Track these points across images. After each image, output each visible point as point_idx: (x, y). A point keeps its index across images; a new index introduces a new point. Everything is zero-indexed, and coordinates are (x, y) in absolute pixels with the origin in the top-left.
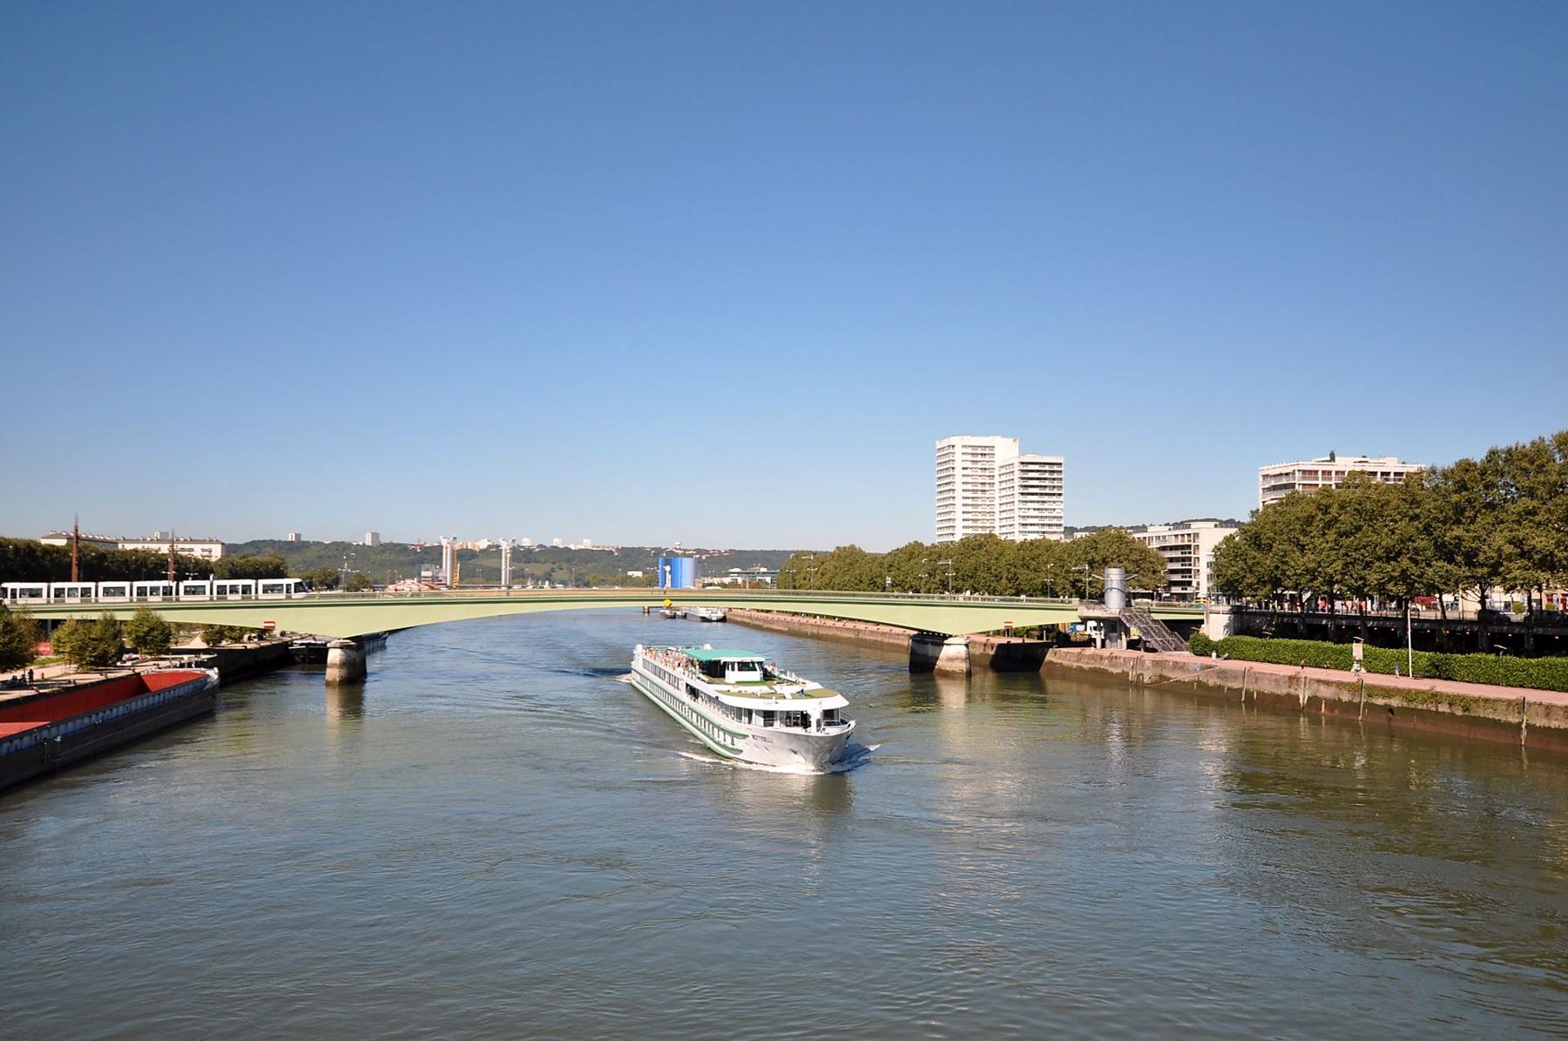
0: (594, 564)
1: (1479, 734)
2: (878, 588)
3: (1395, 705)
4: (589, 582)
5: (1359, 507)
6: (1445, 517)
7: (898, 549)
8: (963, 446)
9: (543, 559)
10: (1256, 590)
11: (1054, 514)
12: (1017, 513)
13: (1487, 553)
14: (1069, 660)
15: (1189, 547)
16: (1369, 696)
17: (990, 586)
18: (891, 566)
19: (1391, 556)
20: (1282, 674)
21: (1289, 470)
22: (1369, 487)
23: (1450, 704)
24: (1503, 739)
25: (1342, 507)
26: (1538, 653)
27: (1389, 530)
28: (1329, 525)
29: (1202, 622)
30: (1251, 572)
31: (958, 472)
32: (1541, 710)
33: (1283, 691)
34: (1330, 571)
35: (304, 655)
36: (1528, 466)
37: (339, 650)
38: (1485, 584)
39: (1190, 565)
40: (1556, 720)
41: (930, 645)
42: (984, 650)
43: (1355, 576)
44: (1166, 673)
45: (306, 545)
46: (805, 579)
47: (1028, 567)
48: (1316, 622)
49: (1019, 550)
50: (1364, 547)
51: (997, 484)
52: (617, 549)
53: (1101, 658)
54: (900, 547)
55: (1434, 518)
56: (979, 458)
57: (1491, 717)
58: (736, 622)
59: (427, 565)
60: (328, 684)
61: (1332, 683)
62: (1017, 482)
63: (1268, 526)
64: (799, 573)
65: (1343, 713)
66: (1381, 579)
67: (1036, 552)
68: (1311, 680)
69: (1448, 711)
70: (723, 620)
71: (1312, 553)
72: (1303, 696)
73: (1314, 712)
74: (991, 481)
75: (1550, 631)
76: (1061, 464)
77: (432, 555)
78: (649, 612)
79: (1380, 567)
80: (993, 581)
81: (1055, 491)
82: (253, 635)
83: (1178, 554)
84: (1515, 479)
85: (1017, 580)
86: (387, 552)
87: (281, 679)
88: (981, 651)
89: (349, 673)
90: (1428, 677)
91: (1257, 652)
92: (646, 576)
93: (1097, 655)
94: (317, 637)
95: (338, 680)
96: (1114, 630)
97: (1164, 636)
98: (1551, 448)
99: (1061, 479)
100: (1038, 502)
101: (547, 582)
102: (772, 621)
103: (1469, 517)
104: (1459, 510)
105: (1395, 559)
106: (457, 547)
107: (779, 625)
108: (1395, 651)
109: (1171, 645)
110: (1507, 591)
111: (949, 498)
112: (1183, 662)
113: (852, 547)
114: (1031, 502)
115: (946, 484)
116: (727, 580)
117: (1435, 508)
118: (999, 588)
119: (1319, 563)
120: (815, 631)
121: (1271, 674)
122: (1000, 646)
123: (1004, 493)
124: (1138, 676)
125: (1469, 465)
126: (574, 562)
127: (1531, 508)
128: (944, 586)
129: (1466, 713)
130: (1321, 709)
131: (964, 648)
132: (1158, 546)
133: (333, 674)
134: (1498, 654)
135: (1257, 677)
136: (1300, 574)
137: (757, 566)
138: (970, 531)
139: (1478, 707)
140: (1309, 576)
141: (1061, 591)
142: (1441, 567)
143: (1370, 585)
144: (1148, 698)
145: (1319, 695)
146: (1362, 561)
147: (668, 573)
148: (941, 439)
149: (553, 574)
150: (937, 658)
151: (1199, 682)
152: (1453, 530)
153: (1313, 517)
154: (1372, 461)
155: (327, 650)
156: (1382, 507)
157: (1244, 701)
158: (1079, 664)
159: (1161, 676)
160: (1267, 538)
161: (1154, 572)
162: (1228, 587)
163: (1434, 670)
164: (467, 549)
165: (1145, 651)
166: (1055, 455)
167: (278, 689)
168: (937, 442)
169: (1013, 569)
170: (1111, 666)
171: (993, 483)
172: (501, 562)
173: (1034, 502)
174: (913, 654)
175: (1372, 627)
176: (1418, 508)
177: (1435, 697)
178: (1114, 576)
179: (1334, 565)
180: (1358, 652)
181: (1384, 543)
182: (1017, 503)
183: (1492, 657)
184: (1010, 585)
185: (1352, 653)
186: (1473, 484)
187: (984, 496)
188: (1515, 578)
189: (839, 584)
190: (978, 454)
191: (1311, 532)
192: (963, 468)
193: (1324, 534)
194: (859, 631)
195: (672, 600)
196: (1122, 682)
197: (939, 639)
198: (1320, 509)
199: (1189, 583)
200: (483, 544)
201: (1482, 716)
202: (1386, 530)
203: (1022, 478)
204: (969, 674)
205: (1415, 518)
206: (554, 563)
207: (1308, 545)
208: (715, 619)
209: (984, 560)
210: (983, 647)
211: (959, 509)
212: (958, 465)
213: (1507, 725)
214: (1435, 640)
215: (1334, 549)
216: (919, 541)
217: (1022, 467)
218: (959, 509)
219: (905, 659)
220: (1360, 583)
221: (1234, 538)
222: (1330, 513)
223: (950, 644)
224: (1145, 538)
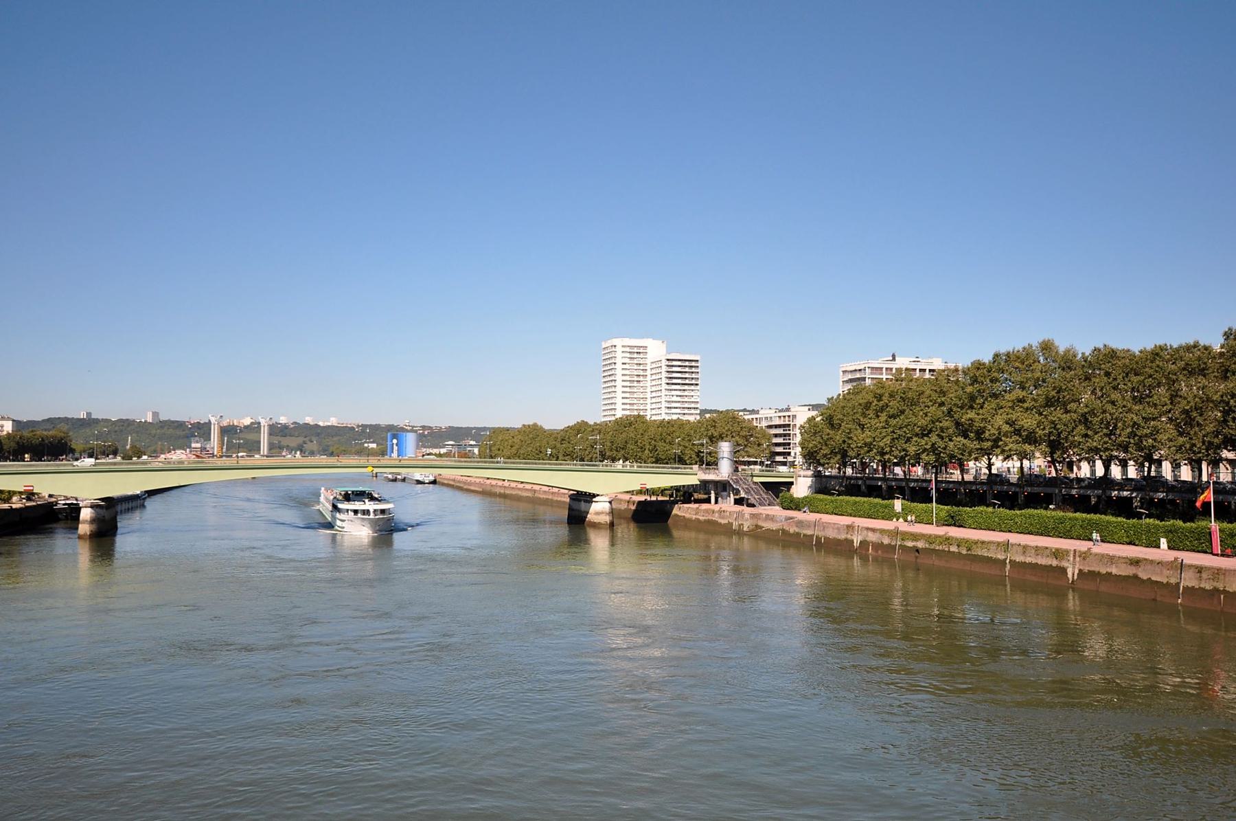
0: (339, 438)
1: (977, 568)
2: (553, 457)
3: (921, 547)
4: (333, 452)
5: (904, 396)
6: (962, 404)
7: (568, 427)
8: (623, 346)
9: (296, 434)
10: (829, 459)
11: (692, 400)
12: (663, 399)
13: (991, 431)
14: (690, 514)
15: (789, 425)
16: (902, 540)
17: (636, 455)
18: (563, 440)
19: (926, 433)
20: (842, 523)
21: (862, 367)
22: (911, 380)
23: (958, 546)
24: (995, 571)
25: (891, 396)
26: (869, 496)
27: (924, 413)
28: (882, 410)
29: (792, 483)
30: (826, 445)
31: (619, 366)
32: (1020, 549)
33: (843, 536)
34: (882, 444)
35: (66, 513)
36: (1020, 366)
37: (90, 509)
38: (988, 453)
39: (790, 439)
40: (1030, 556)
41: (582, 502)
42: (628, 505)
43: (899, 448)
44: (761, 523)
45: (97, 421)
46: (499, 450)
47: (665, 442)
48: (873, 483)
49: (658, 427)
50: (906, 426)
51: (649, 376)
52: (358, 426)
53: (713, 512)
54: (571, 425)
55: (955, 404)
56: (635, 356)
57: (986, 555)
58: (443, 484)
59: (197, 439)
60: (80, 537)
61: (877, 530)
62: (664, 375)
63: (838, 410)
64: (495, 445)
65: (883, 553)
66: (917, 451)
67: (671, 429)
68: (862, 528)
69: (957, 551)
70: (434, 482)
71: (870, 431)
72: (856, 540)
73: (864, 552)
74: (645, 374)
75: (1036, 490)
76: (697, 361)
77: (202, 430)
78: (376, 476)
79: (917, 442)
80: (639, 452)
81: (693, 382)
82: (23, 497)
83: (780, 431)
84: (1011, 375)
85: (656, 451)
86: (166, 428)
87: (50, 532)
88: (626, 507)
89: (98, 528)
90: (947, 525)
91: (827, 507)
92: (380, 447)
93: (710, 509)
94: (79, 499)
95: (88, 534)
96: (725, 490)
97: (761, 495)
98: (1036, 352)
99: (698, 373)
100: (680, 390)
101: (298, 453)
102: (470, 484)
103: (979, 404)
104: (972, 398)
105: (927, 435)
106: (225, 423)
107: (475, 487)
108: (924, 505)
109: (766, 501)
110: (1005, 459)
111: (611, 386)
112: (774, 514)
113: (535, 425)
114: (675, 390)
115: (610, 375)
116: (443, 451)
117: (955, 397)
118: (643, 457)
119: (874, 438)
120: (502, 491)
121: (834, 524)
122: (640, 503)
123: (654, 383)
124: (740, 525)
125: (980, 364)
126: (323, 436)
127: (1021, 397)
128: (603, 457)
129: (969, 552)
130: (869, 550)
131: (608, 504)
132: (766, 425)
133: (84, 528)
134: (994, 508)
135: (825, 526)
136: (861, 447)
137: (468, 439)
138: (628, 413)
139: (977, 547)
140: (866, 448)
141: (688, 459)
142: (959, 442)
143: (909, 455)
144: (747, 543)
145: (868, 539)
146: (905, 437)
147: (395, 445)
148: (605, 341)
149: (305, 445)
150: (588, 513)
151: (783, 530)
152: (967, 413)
153: (871, 403)
154: (924, 361)
155: (80, 508)
156: (919, 395)
157: (815, 545)
158: (697, 517)
159: (756, 526)
160: (838, 419)
161: (759, 445)
162: (811, 457)
163: (951, 520)
164: (233, 425)
165: (747, 506)
166: (687, 354)
167: (47, 541)
168: (603, 343)
169: (653, 442)
170: (720, 518)
171: (646, 375)
172: (260, 436)
173: (677, 390)
174: (570, 509)
175: (913, 488)
176: (944, 396)
177: (948, 540)
178: (725, 448)
179: (885, 440)
180: (898, 506)
181: (919, 424)
182: (663, 391)
183: (990, 509)
184: (651, 455)
185: (893, 507)
186: (982, 379)
188: (1010, 450)
189: (524, 454)
190: (634, 353)
191: (869, 414)
192: (623, 364)
193: (878, 416)
194: (535, 491)
195: (373, 467)
196: (728, 531)
197: (589, 497)
198: (876, 397)
199: (789, 454)
200: (247, 421)
201: (979, 554)
202: (921, 413)
203: (668, 372)
204: (612, 525)
205: (942, 404)
206: (305, 437)
207: (866, 424)
208: (428, 482)
209: (632, 435)
210: (627, 504)
211: (619, 395)
212: (619, 361)
213: (996, 561)
214: (957, 497)
215: (885, 428)
216: (585, 420)
217: (667, 363)
218: (619, 395)
219: (565, 513)
220: (903, 453)
221: (815, 419)
222: (882, 401)
223: (597, 502)
224: (753, 419)
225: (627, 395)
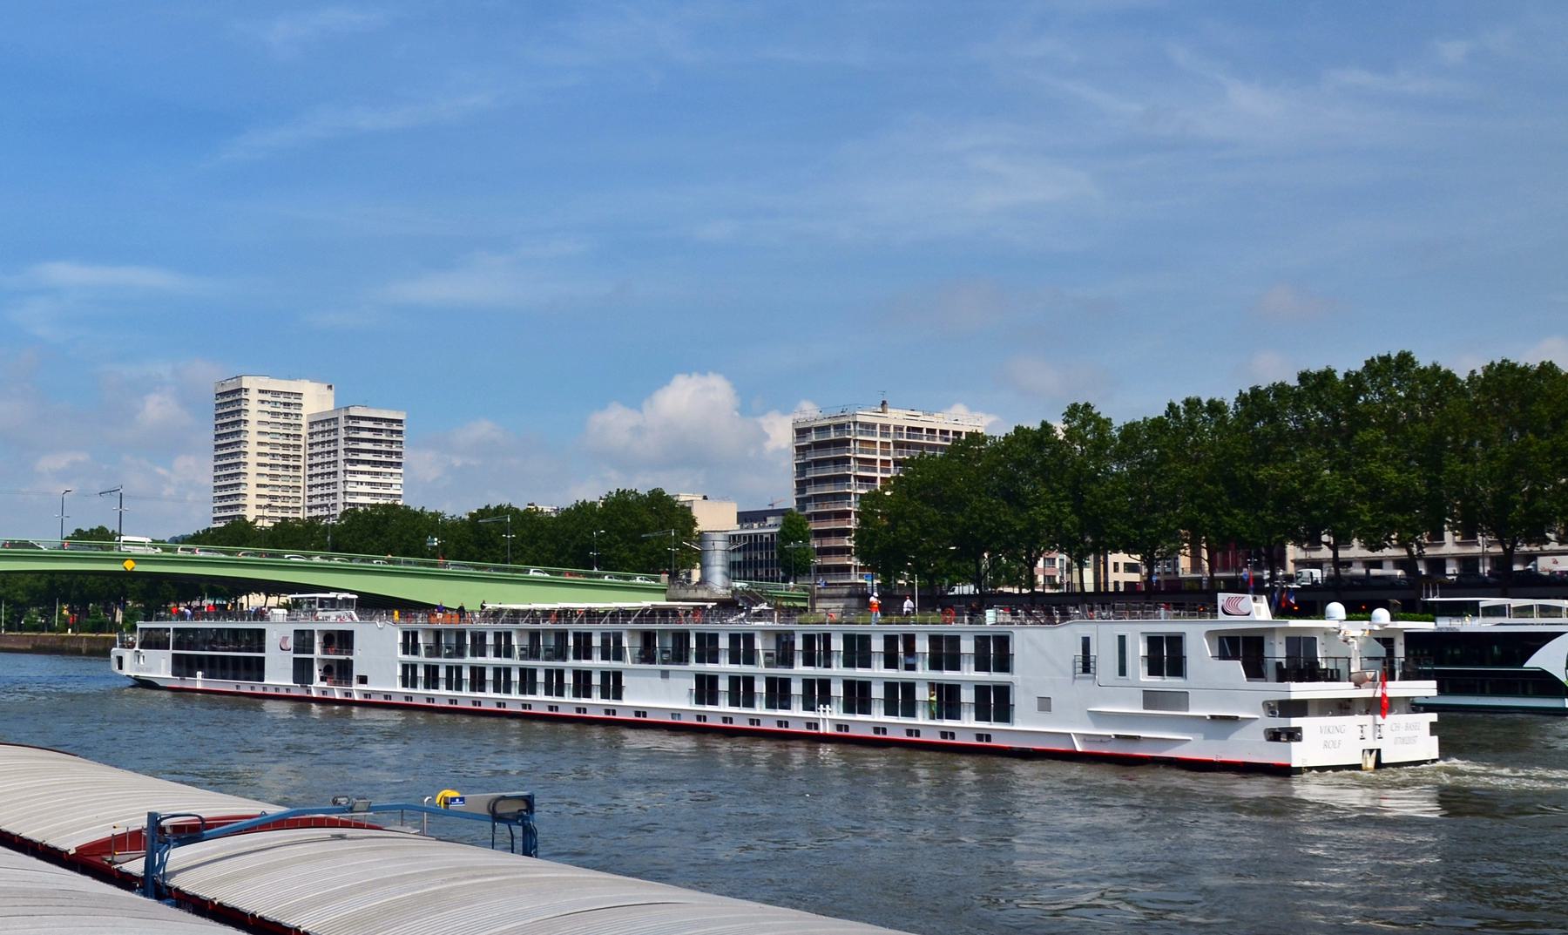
8: (260, 391)
11: (391, 491)
24: (1107, 739)
99: (401, 442)
187: (286, 473)
225: (266, 481)
